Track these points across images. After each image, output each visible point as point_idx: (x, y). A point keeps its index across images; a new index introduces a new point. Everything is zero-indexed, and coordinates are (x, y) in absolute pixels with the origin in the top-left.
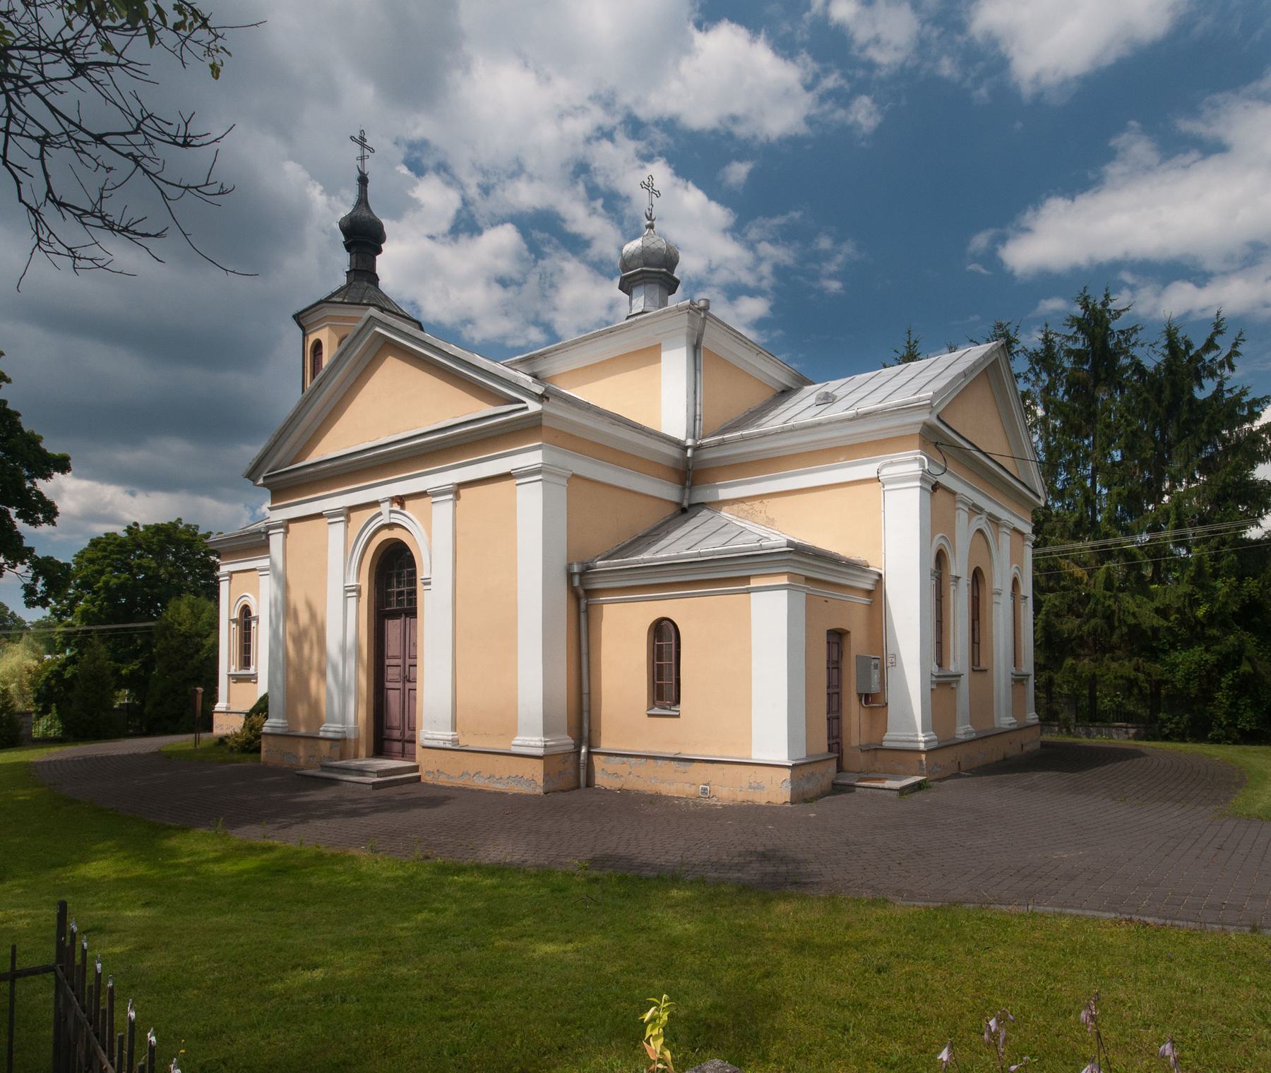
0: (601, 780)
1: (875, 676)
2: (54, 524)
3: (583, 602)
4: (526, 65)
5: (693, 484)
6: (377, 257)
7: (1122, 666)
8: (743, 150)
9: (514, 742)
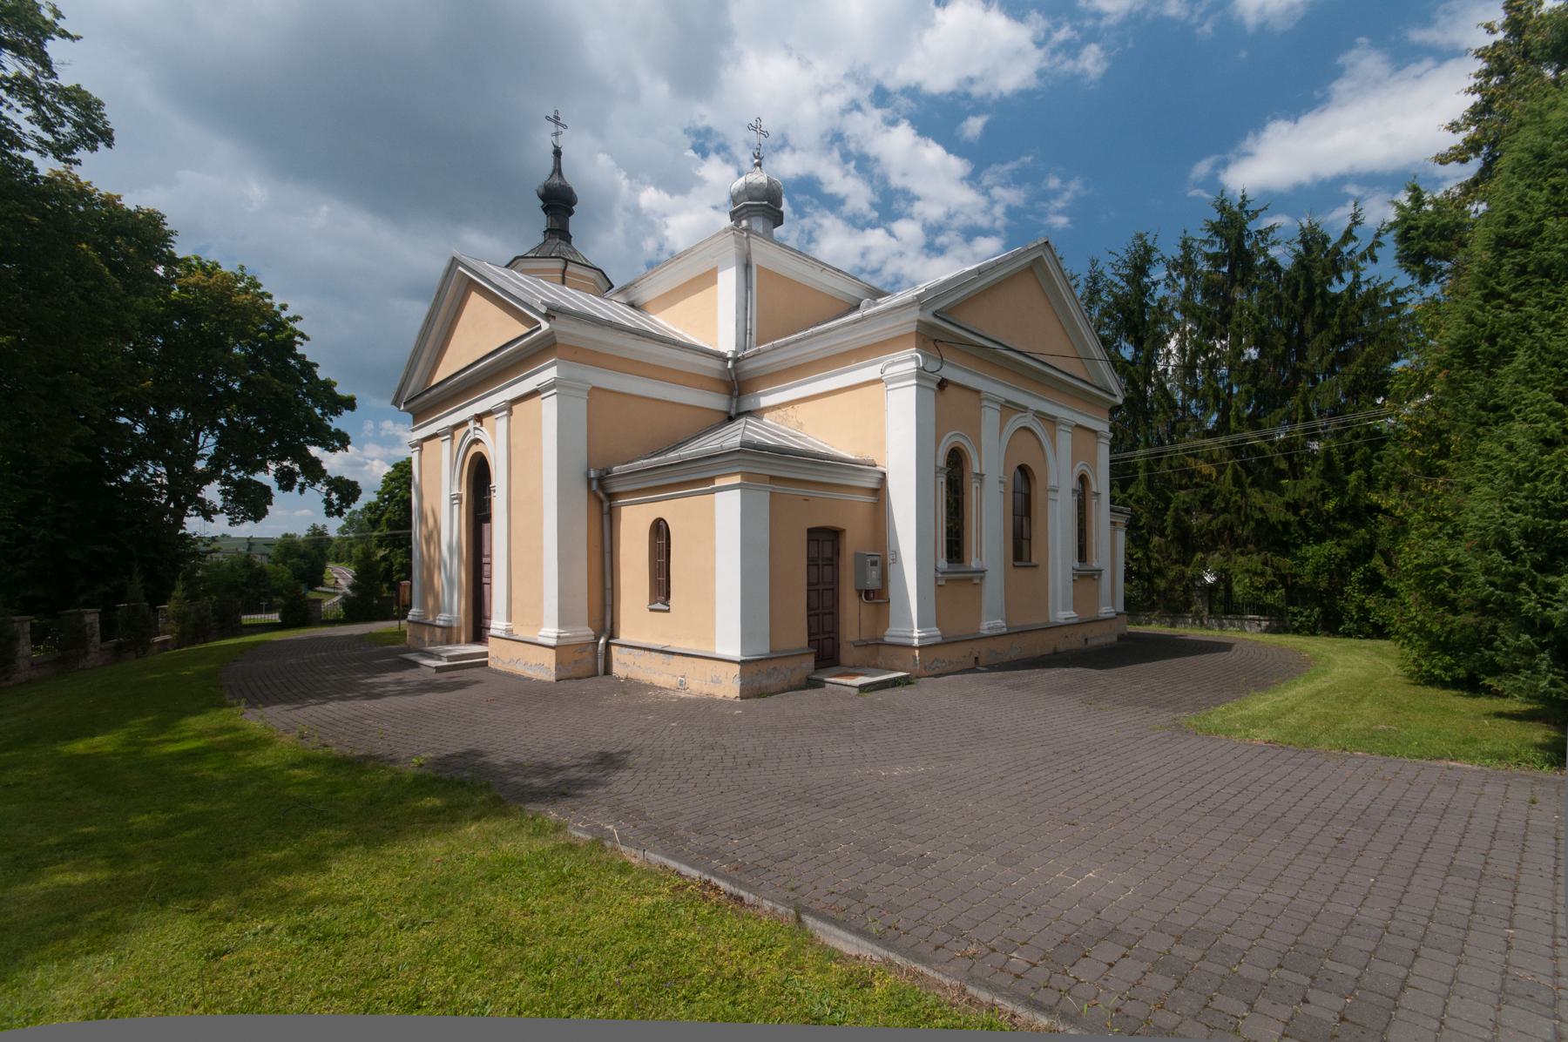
0: (618, 670)
1: (874, 574)
2: (347, 451)
3: (606, 504)
4: (790, 55)
5: (740, 395)
6: (570, 218)
7: (1250, 560)
8: (978, 107)
9: (541, 633)
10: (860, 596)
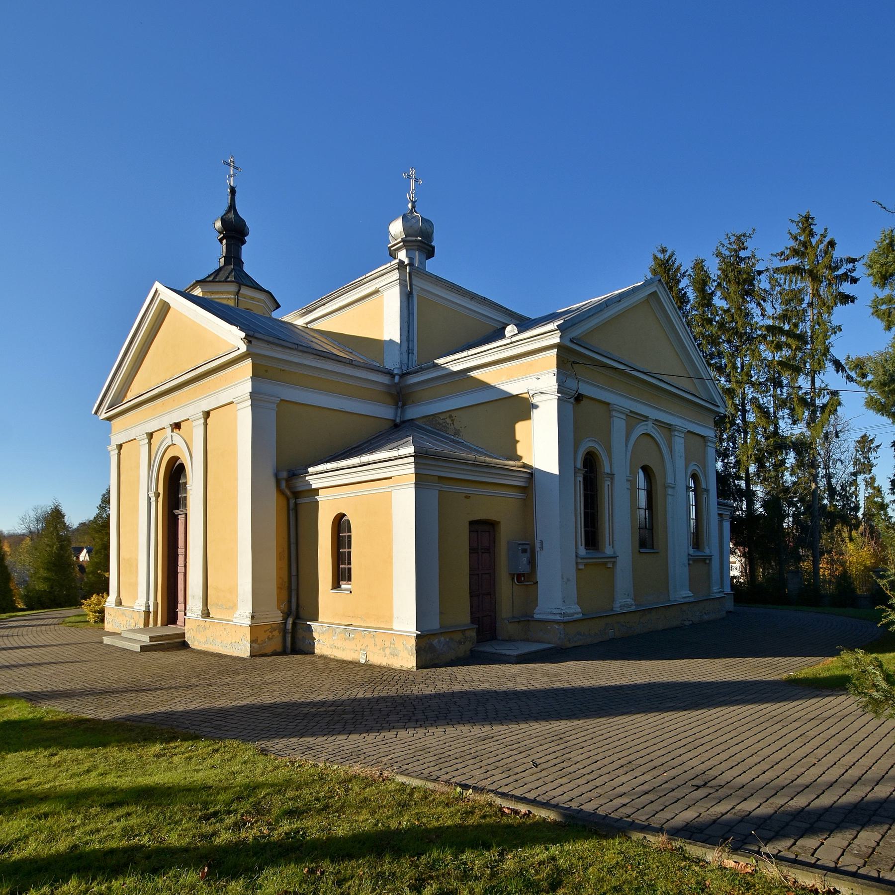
5: (404, 405)
10: (513, 579)
